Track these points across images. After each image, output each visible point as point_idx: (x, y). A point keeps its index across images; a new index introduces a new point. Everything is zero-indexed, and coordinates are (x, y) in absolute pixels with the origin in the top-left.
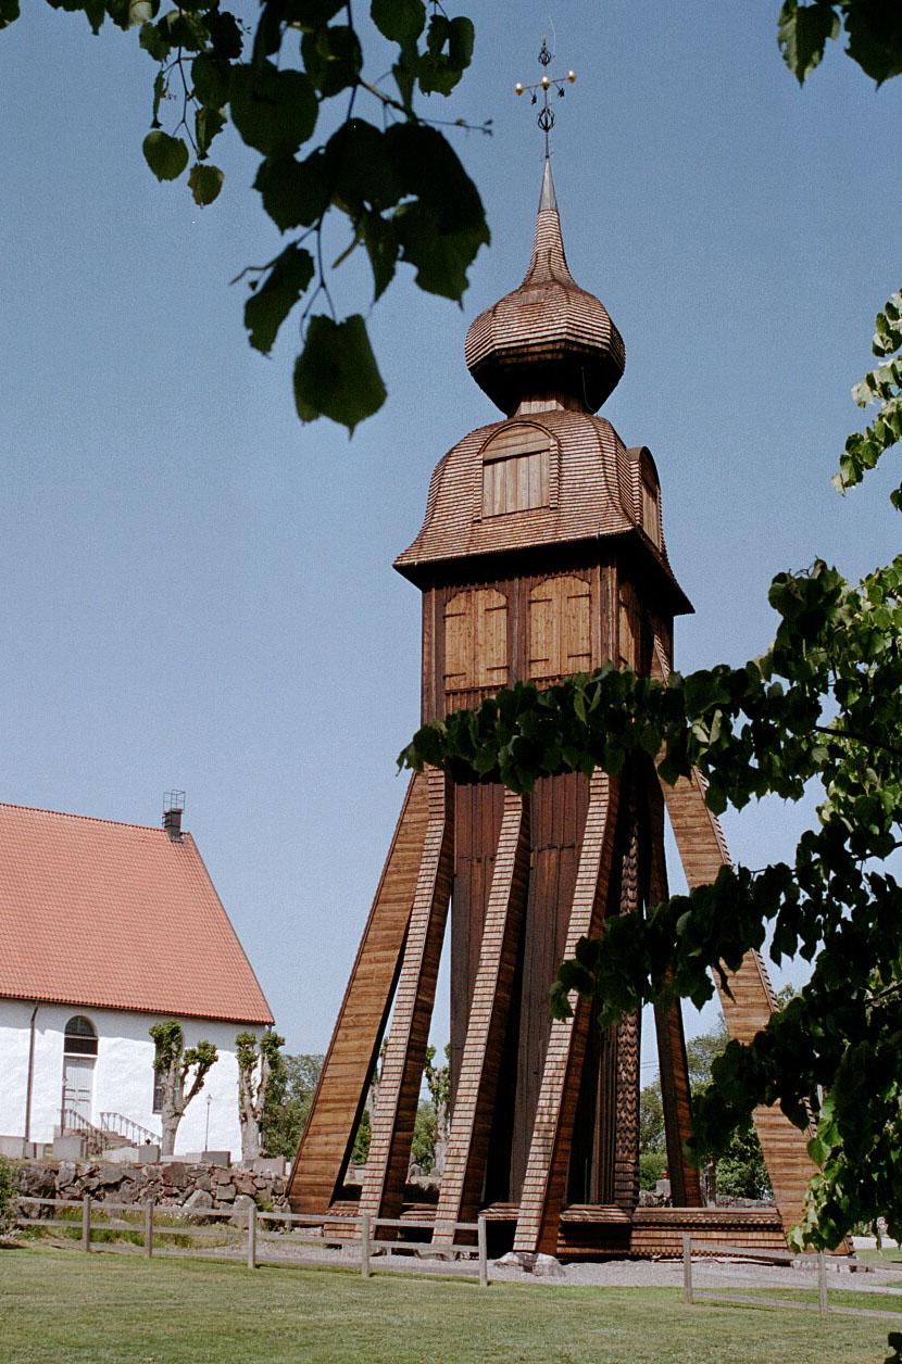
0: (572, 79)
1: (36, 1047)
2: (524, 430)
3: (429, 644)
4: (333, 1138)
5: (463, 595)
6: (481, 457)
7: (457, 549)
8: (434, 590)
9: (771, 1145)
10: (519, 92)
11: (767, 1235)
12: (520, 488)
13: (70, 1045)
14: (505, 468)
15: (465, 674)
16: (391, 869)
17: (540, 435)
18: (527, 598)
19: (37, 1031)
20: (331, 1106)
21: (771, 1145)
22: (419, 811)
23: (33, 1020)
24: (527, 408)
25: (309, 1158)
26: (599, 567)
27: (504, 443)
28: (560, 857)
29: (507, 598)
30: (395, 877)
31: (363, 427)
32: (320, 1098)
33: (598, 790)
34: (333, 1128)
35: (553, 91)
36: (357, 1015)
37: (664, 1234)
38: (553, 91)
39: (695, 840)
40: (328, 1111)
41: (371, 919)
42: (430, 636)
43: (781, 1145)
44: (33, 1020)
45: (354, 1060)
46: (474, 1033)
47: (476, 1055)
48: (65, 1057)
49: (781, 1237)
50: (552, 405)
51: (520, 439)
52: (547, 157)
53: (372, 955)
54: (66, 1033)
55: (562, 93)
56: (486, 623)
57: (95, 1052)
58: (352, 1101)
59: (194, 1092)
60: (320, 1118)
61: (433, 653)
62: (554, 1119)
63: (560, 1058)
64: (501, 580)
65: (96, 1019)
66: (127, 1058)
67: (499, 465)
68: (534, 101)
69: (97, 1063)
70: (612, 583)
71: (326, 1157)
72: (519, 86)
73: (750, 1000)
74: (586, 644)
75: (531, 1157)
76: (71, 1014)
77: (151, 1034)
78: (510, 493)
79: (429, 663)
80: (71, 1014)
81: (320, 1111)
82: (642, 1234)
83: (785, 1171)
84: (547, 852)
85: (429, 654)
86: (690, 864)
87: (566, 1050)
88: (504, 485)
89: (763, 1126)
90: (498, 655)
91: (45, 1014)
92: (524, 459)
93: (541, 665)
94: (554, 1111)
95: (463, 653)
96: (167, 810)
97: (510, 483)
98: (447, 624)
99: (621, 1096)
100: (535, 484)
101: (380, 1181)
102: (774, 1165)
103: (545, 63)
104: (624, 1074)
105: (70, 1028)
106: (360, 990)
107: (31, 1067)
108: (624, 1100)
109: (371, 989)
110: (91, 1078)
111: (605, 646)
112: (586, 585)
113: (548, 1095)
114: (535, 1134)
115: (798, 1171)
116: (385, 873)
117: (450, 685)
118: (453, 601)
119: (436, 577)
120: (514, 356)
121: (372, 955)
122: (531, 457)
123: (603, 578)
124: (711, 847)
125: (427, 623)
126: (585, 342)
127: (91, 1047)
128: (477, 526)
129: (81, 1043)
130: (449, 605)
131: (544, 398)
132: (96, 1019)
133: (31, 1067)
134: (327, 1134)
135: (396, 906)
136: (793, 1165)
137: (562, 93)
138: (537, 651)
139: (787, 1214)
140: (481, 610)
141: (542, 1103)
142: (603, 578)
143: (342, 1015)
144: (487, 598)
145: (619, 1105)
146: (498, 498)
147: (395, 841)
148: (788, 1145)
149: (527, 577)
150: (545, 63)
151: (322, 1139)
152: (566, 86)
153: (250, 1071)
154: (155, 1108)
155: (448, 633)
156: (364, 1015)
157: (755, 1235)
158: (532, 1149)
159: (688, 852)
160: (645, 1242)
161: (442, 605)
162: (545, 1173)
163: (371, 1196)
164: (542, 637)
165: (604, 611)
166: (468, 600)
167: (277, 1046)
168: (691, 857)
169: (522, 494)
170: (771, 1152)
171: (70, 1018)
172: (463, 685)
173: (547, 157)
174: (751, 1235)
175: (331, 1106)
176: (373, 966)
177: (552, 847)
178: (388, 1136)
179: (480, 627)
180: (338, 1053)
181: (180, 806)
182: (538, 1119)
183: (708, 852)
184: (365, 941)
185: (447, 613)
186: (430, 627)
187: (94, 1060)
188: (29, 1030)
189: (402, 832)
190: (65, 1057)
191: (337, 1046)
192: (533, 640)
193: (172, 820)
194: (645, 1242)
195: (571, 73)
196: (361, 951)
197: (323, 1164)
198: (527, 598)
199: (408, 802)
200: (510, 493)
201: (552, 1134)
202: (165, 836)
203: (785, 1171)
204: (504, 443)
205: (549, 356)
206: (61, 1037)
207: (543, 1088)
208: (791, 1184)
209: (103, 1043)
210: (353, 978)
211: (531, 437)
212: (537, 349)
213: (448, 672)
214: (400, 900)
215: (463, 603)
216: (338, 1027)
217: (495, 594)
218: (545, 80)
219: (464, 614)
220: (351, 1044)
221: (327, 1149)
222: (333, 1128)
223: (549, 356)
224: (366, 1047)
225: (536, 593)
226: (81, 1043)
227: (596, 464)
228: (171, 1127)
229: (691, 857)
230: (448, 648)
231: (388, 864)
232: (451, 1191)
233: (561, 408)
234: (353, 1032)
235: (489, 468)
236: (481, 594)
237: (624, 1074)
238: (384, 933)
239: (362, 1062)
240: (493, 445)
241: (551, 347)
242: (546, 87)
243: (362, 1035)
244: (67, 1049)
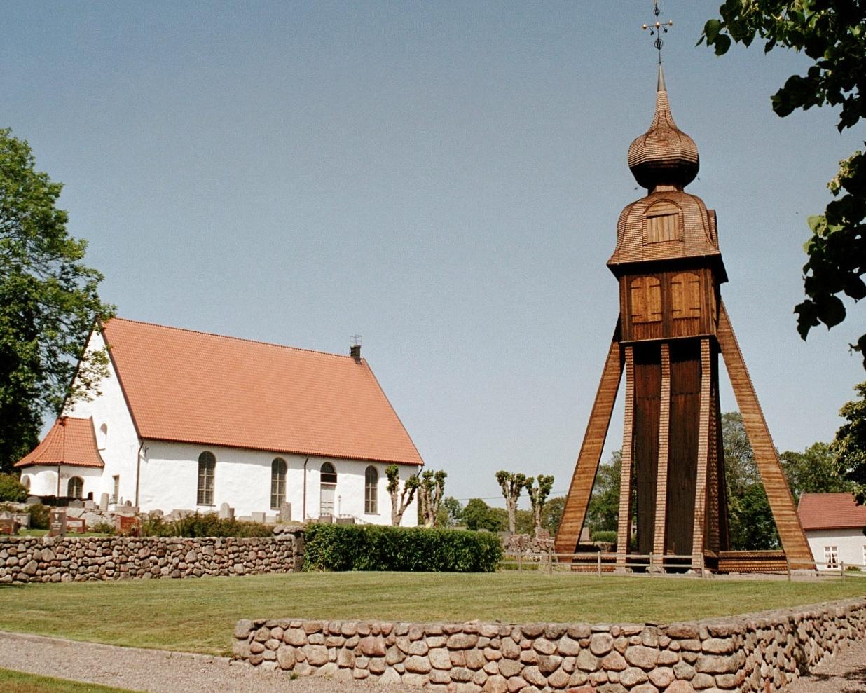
0: (671, 24)
1: (307, 479)
2: (666, 203)
3: (624, 301)
4: (574, 524)
5: (639, 279)
6: (645, 215)
7: (636, 258)
8: (625, 276)
9: (780, 523)
10: (645, 28)
11: (779, 562)
12: (665, 230)
13: (324, 478)
14: (657, 221)
15: (641, 315)
16: (598, 401)
17: (673, 206)
18: (669, 282)
19: (307, 471)
20: (572, 509)
21: (780, 523)
22: (611, 375)
23: (305, 464)
24: (659, 189)
25: (563, 533)
26: (703, 270)
27: (656, 209)
28: (685, 398)
29: (660, 281)
30: (601, 405)
31: (835, 328)
32: (568, 505)
33: (706, 369)
34: (575, 520)
35: (661, 29)
36: (585, 468)
37: (733, 562)
38: (661, 29)
39: (742, 390)
40: (571, 512)
41: (589, 423)
42: (624, 297)
43: (784, 523)
44: (305, 464)
45: (583, 488)
46: (661, 477)
47: (663, 486)
48: (322, 485)
49: (785, 562)
50: (671, 188)
51: (664, 208)
52: (660, 63)
53: (591, 440)
54: (321, 471)
55: (666, 31)
56: (651, 293)
57: (335, 481)
58: (583, 507)
59: (409, 502)
60: (568, 515)
61: (626, 304)
62: (703, 513)
63: (702, 487)
64: (658, 273)
65: (335, 464)
66: (351, 482)
67: (654, 219)
68: (652, 33)
69: (337, 487)
70: (709, 277)
71: (571, 533)
72: (645, 26)
73: (769, 460)
74: (698, 304)
75: (695, 530)
76: (323, 461)
77: (386, 472)
78: (660, 232)
79: (624, 310)
80: (323, 461)
81: (568, 512)
82: (723, 563)
83: (787, 534)
84: (680, 396)
85: (624, 305)
86: (740, 400)
87: (705, 484)
88: (657, 228)
89: (776, 515)
90: (657, 307)
91: (311, 461)
92: (666, 217)
93: (678, 312)
94: (703, 510)
95: (640, 305)
96: (353, 346)
97: (660, 228)
98: (632, 293)
99: (712, 503)
100: (672, 229)
101: (625, 542)
102: (782, 532)
103: (657, 15)
104: (713, 493)
105: (323, 469)
106: (585, 457)
107: (305, 491)
108: (713, 505)
109: (590, 456)
110: (334, 495)
111: (707, 305)
112: (697, 277)
113: (699, 500)
114: (695, 520)
115: (792, 534)
116: (596, 403)
117: (635, 320)
118: (635, 281)
119: (624, 272)
120: (655, 165)
121: (591, 440)
122: (669, 217)
123: (705, 274)
124: (749, 393)
125: (622, 291)
126: (688, 160)
127: (334, 479)
128: (645, 247)
129: (329, 477)
130: (633, 283)
131: (667, 184)
132: (287, 459)
133: (305, 491)
134: (571, 522)
135: (601, 418)
136: (790, 531)
137: (666, 31)
138: (676, 306)
139: (788, 552)
140: (648, 287)
141: (697, 507)
142: (705, 274)
143: (577, 468)
144: (650, 281)
145: (711, 507)
146: (654, 234)
147: (600, 388)
148: (787, 523)
149: (670, 272)
150: (657, 15)
151: (569, 525)
152: (667, 27)
153: (431, 491)
154: (272, 506)
155: (633, 296)
156: (587, 468)
157: (773, 562)
158: (695, 526)
159: (739, 395)
160: (724, 566)
161: (629, 283)
162: (702, 536)
163: (622, 548)
164: (678, 300)
165: (706, 289)
166: (642, 281)
167: (443, 477)
168: (741, 398)
169: (666, 234)
170: (780, 526)
171: (202, 452)
172: (640, 321)
173: (660, 63)
174: (772, 562)
175: (572, 509)
176: (591, 446)
177: (681, 394)
178: (627, 522)
179: (648, 293)
180: (575, 486)
181: (358, 344)
182: (696, 513)
183: (749, 395)
184: (587, 434)
185: (632, 286)
186: (624, 293)
187: (335, 486)
188: (303, 470)
189: (603, 384)
190: (322, 485)
191: (575, 482)
192: (673, 301)
193: (355, 352)
194: (724, 566)
195: (671, 22)
196: (585, 439)
197: (570, 536)
198: (669, 282)
199: (605, 370)
200: (660, 232)
201: (703, 520)
202: (352, 360)
203: (787, 534)
204: (656, 209)
205: (672, 166)
206: (319, 473)
207: (696, 500)
208: (790, 539)
209: (340, 476)
210: (582, 451)
211: (669, 207)
212: (666, 162)
213: (633, 314)
214: (603, 415)
215: (639, 283)
216: (575, 473)
217: (654, 279)
218: (658, 24)
219: (640, 288)
220: (582, 481)
221: (571, 529)
222: (575, 520)
223: (672, 166)
224: (589, 483)
225: (674, 280)
226: (329, 477)
227: (699, 220)
228: (397, 521)
229: (741, 398)
230: (633, 303)
231: (597, 399)
232: (659, 545)
233: (676, 190)
234: (582, 476)
235: (649, 220)
236: (648, 279)
237: (713, 493)
238: (596, 430)
239: (587, 489)
240: (651, 209)
241: (672, 162)
242: (658, 27)
243: (587, 477)
244: (322, 480)
